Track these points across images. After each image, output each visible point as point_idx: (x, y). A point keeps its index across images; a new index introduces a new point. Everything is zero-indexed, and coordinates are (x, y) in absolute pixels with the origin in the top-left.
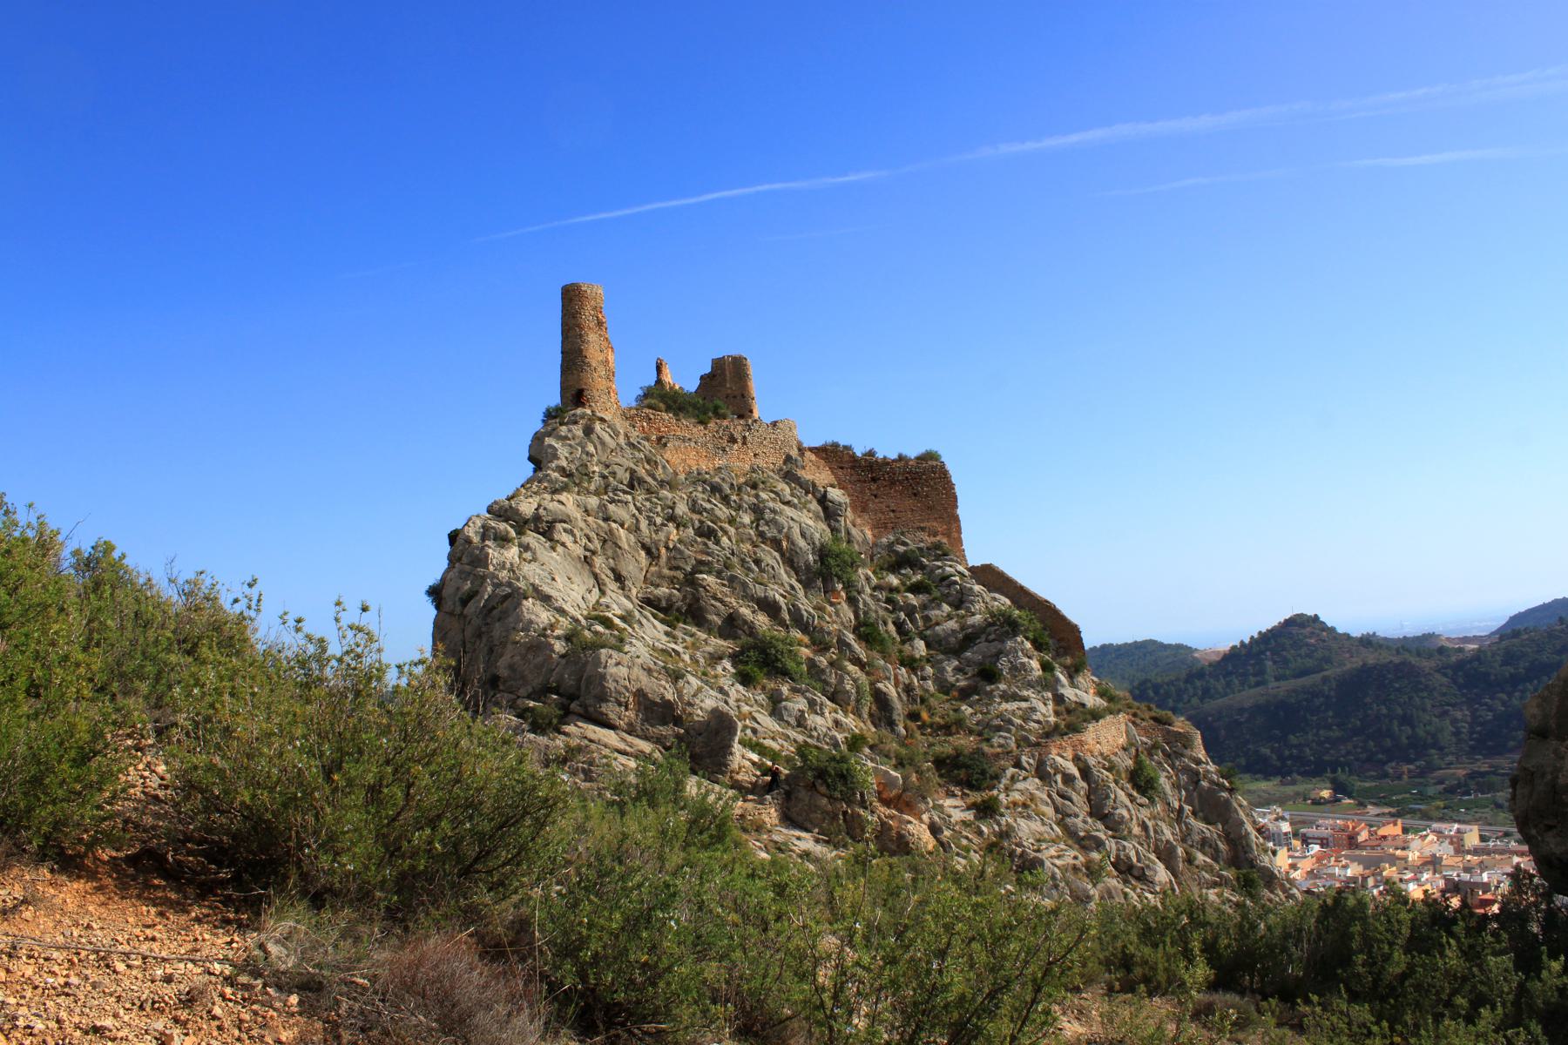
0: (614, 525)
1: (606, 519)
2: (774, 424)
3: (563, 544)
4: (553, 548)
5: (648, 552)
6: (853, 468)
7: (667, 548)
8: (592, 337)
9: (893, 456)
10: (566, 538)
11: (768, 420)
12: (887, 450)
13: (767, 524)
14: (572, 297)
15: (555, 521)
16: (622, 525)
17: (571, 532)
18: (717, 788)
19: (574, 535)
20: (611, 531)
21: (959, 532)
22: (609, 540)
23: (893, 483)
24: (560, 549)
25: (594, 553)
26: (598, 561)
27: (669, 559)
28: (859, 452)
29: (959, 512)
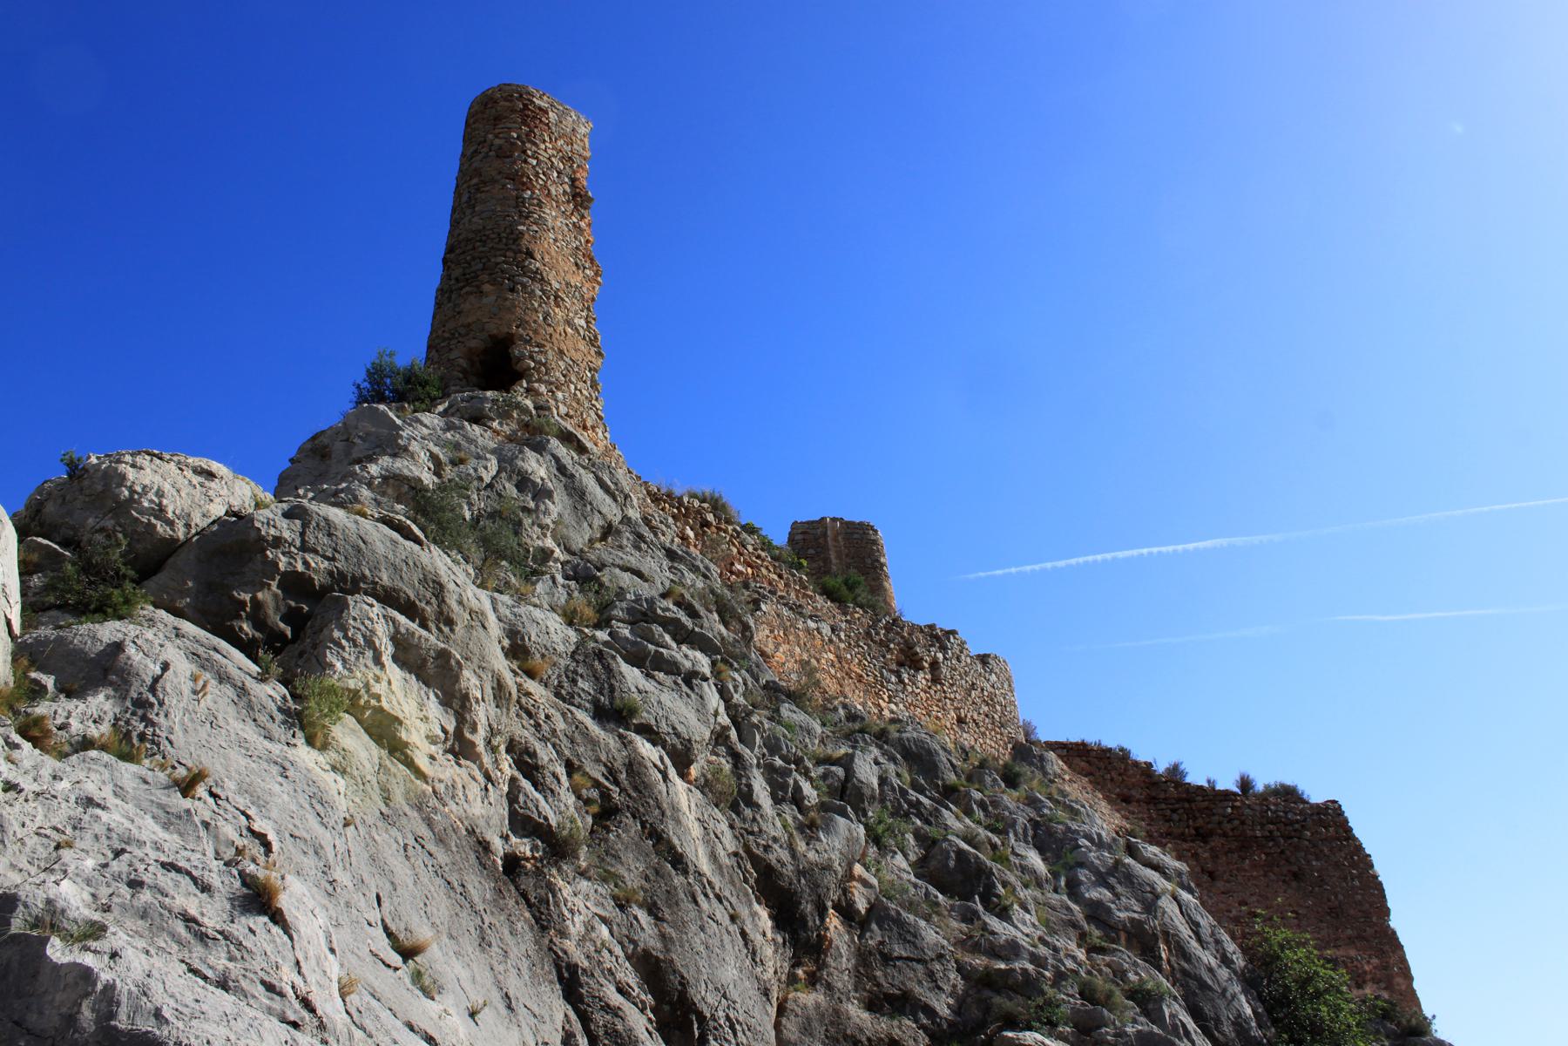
0: (648, 751)
1: (615, 714)
2: (984, 659)
3: (384, 730)
4: (302, 720)
5: (787, 916)
6: (1152, 800)
7: (847, 912)
8: (554, 217)
9: (1227, 782)
10: (399, 693)
11: (975, 649)
12: (1212, 767)
13: (1102, 880)
14: (498, 130)
15: (349, 583)
16: (682, 759)
17: (437, 673)
18: (251, 1013)
19: (456, 702)
20: (634, 766)
21: (1409, 978)
22: (620, 803)
23: (1245, 845)
24: (348, 734)
25: (557, 847)
26: (580, 900)
27: (863, 958)
28: (1161, 767)
29: (1395, 922)
